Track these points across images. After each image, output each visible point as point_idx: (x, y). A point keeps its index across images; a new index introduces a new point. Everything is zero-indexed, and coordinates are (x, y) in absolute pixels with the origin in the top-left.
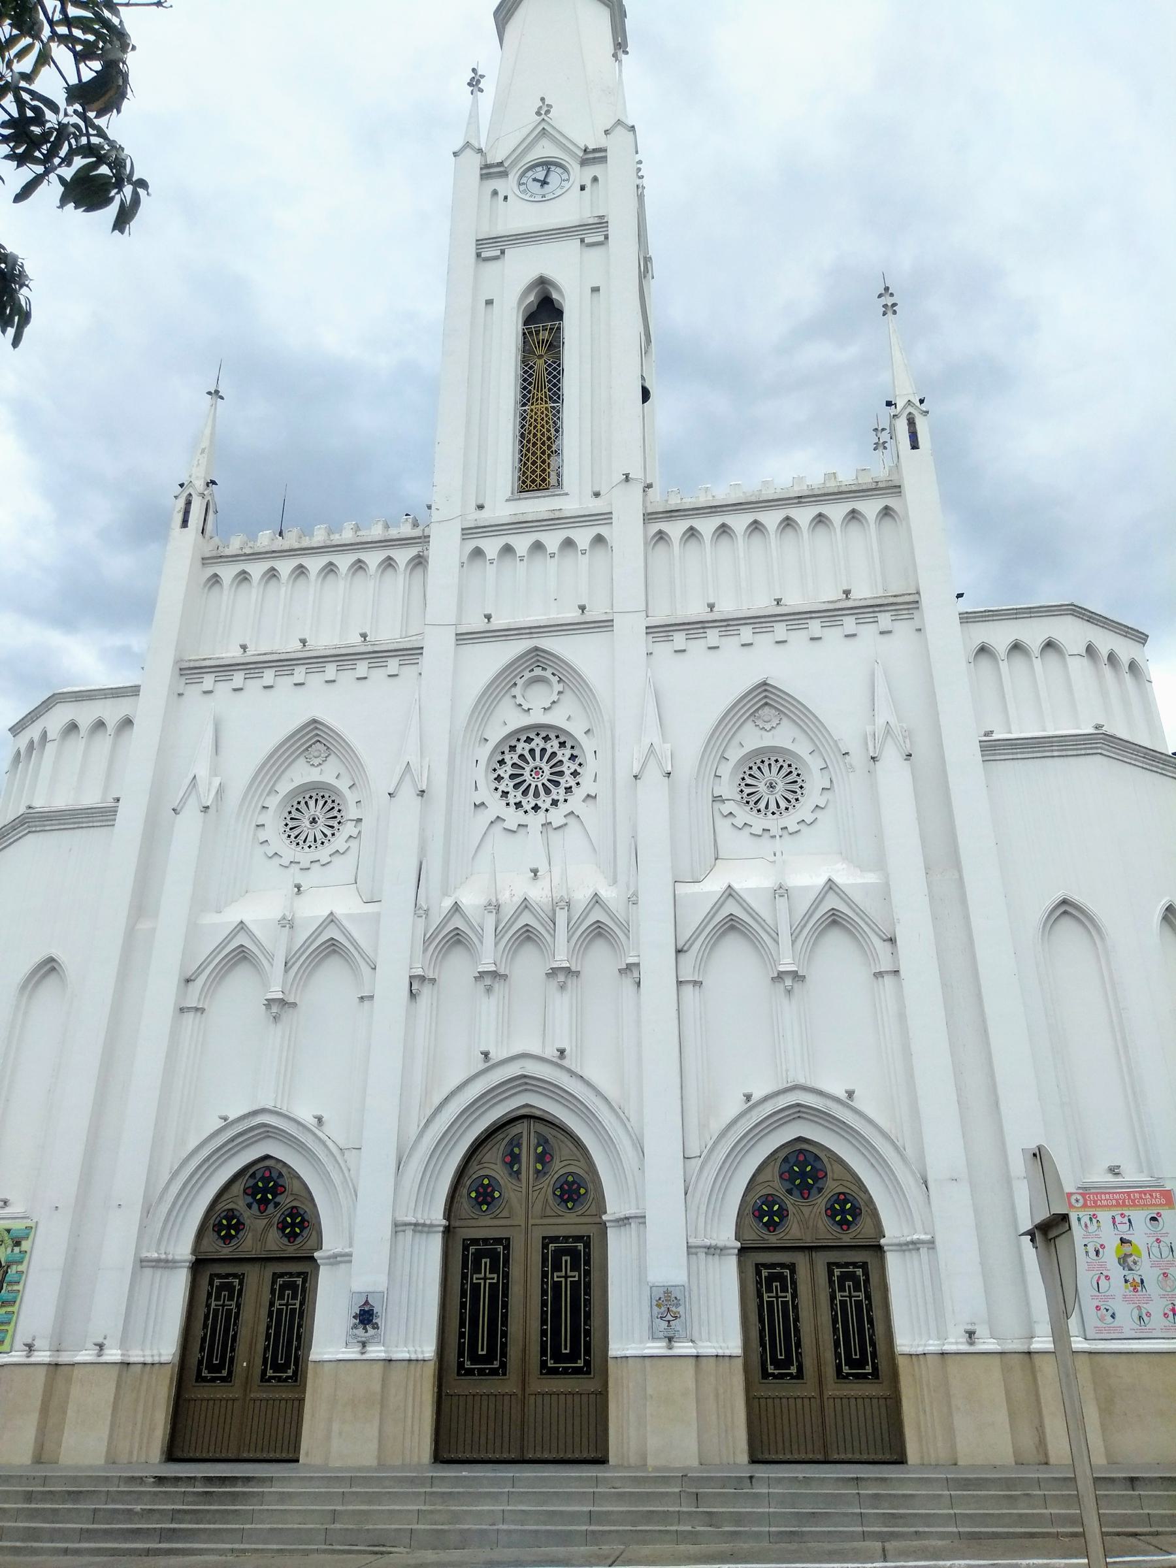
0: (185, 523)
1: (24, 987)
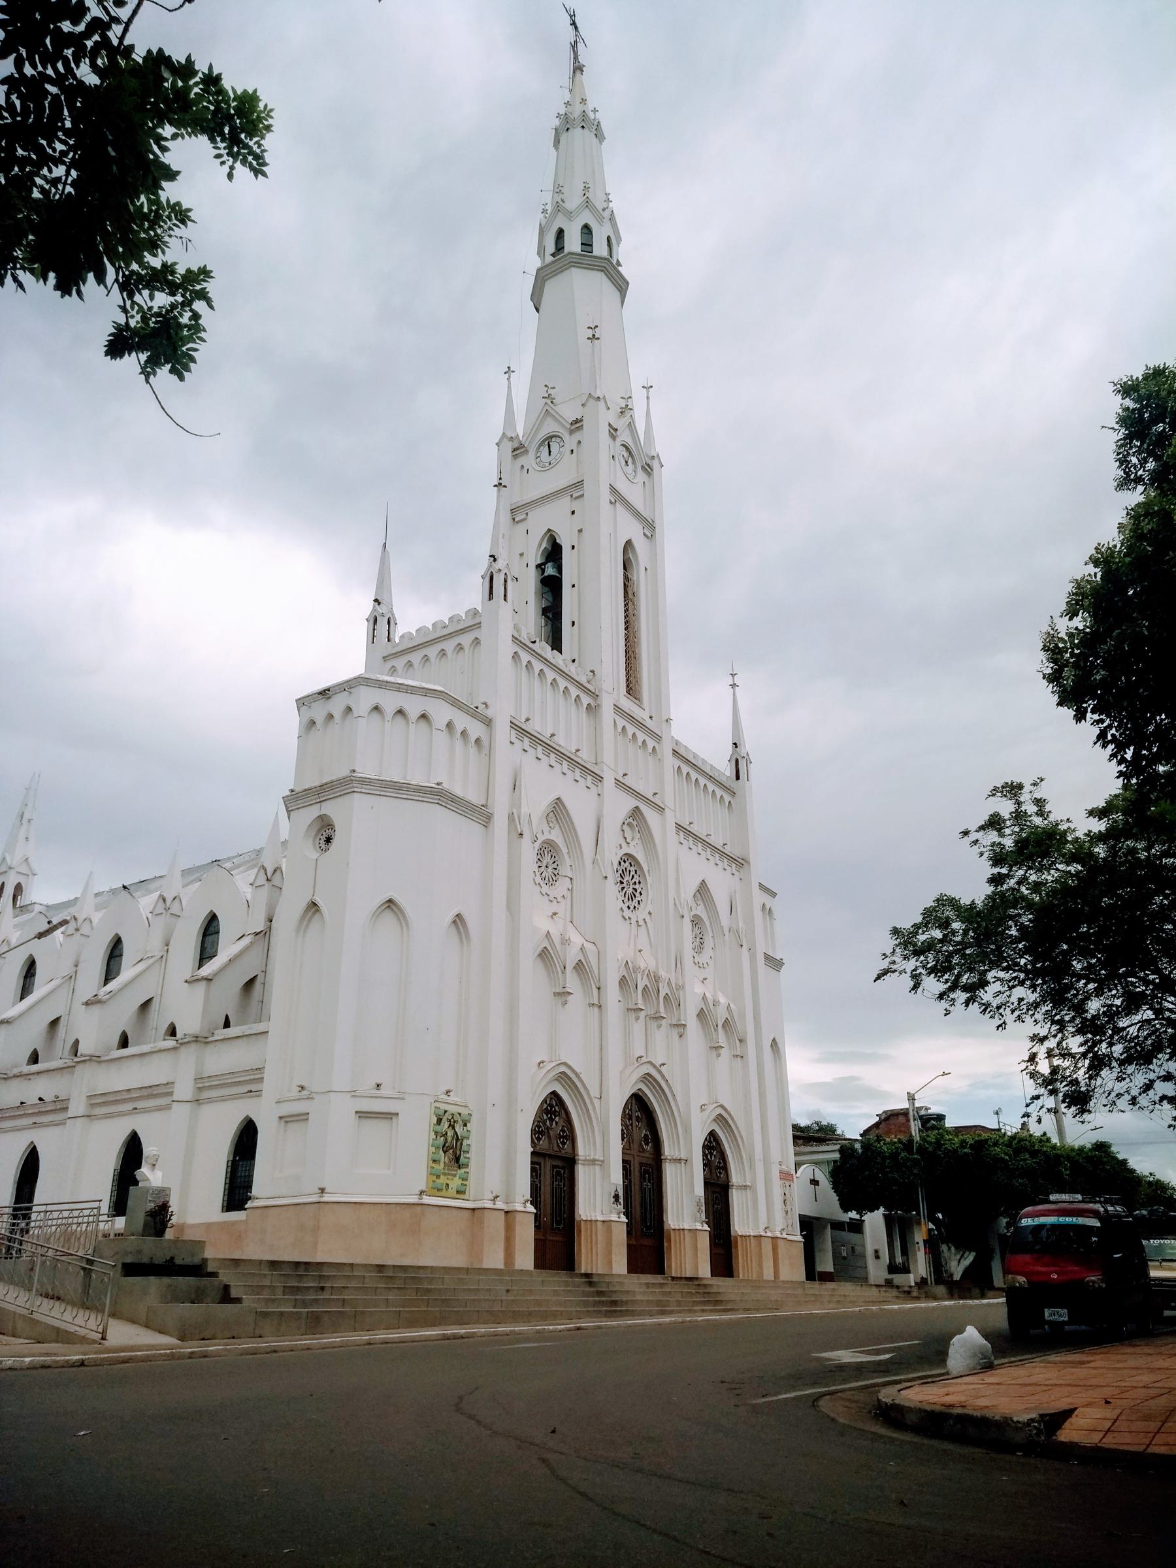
1: (298, 930)
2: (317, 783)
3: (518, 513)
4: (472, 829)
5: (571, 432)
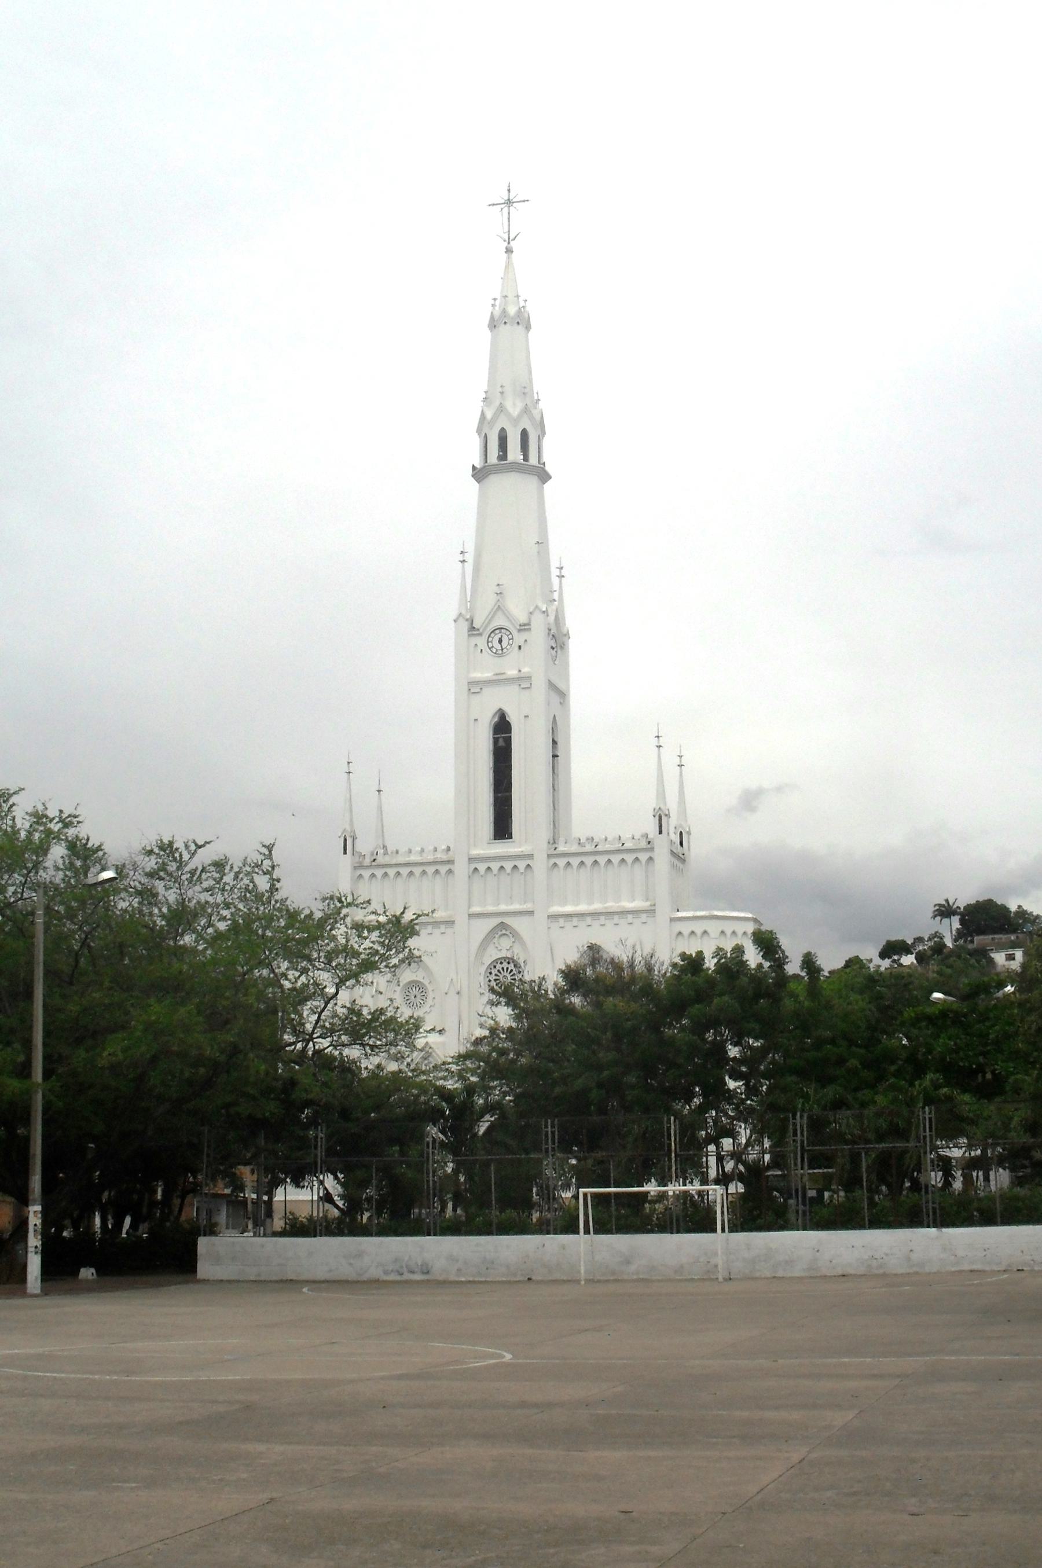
0: (345, 853)
3: (475, 687)
5: (519, 631)
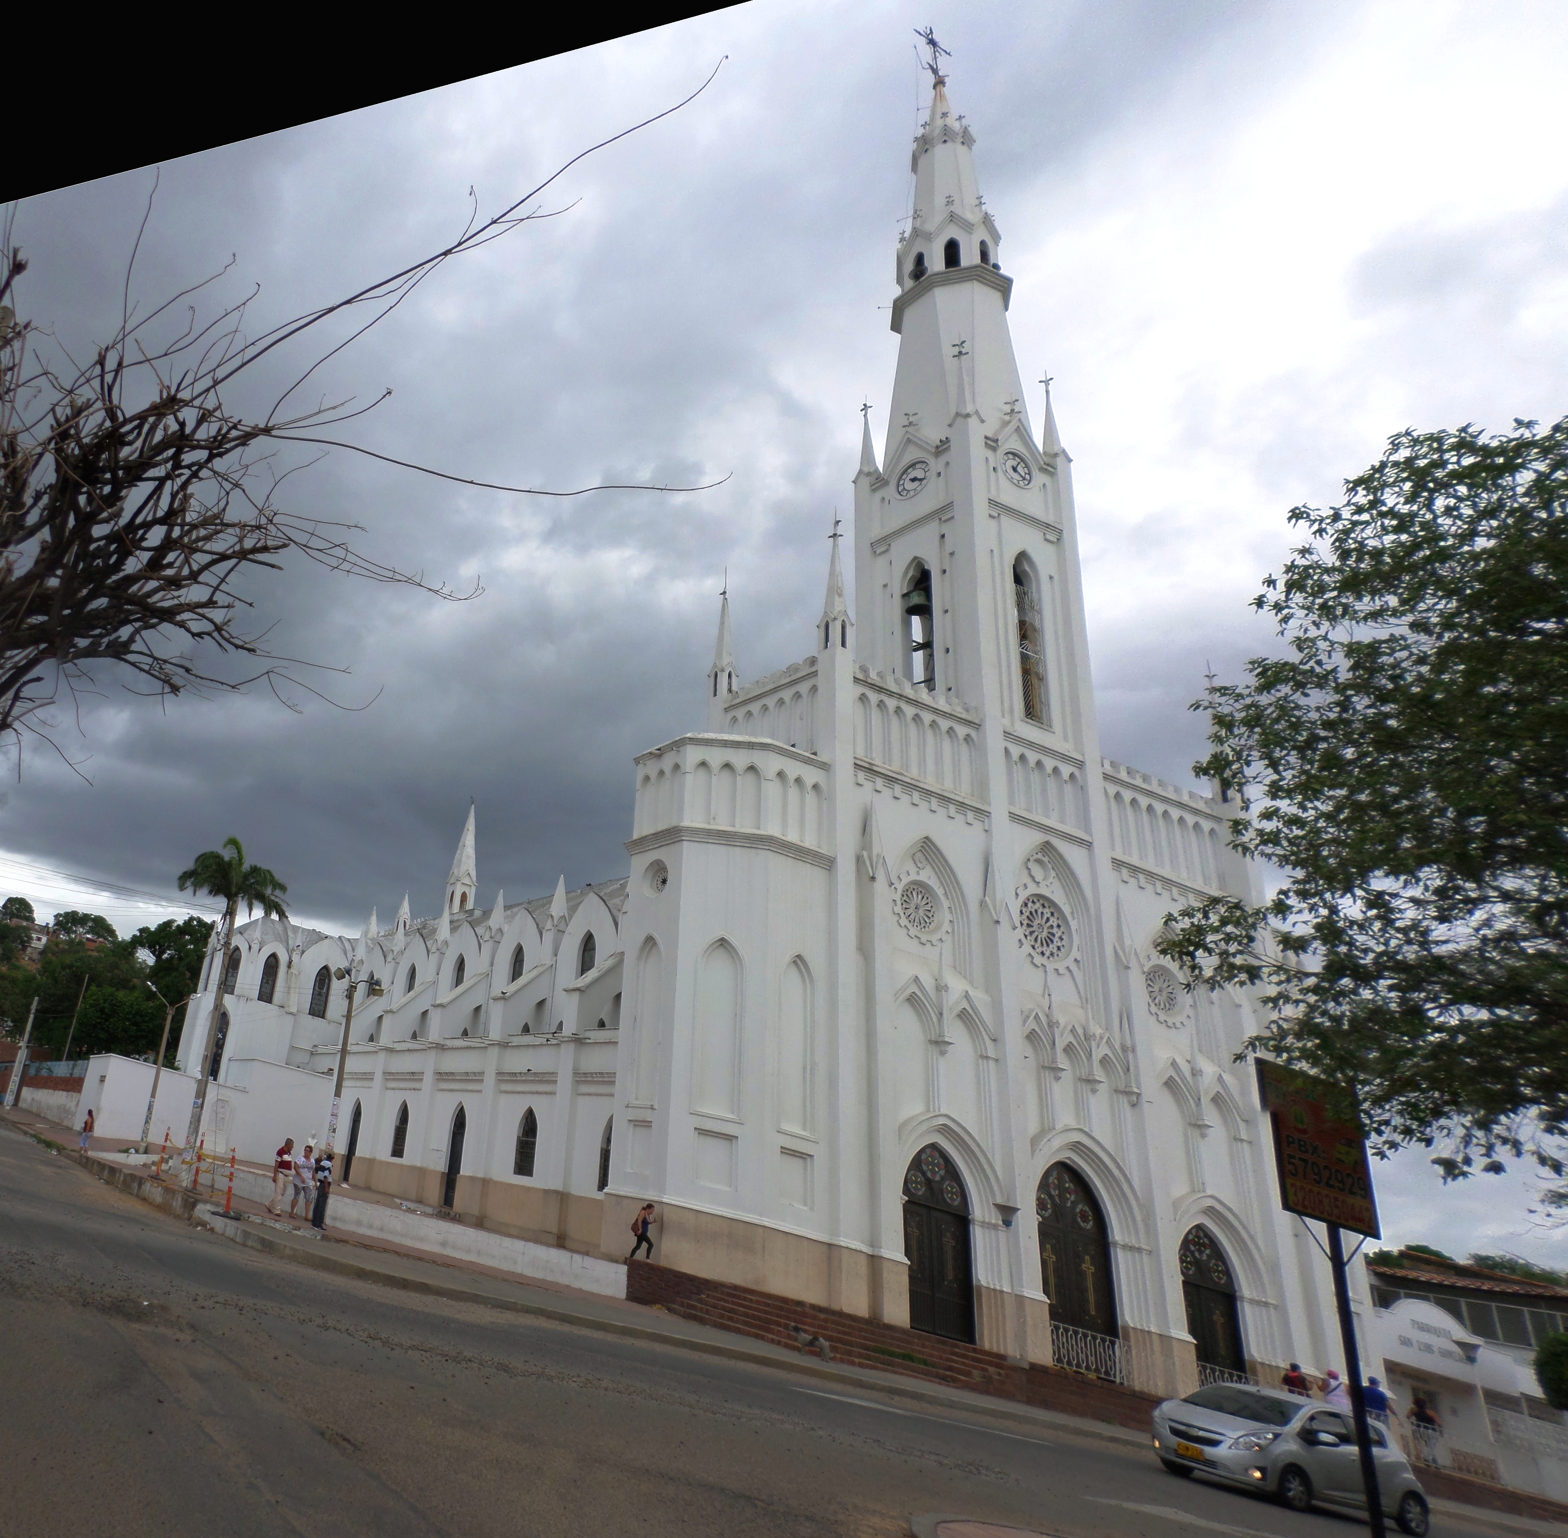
2: (652, 831)
4: (813, 875)
